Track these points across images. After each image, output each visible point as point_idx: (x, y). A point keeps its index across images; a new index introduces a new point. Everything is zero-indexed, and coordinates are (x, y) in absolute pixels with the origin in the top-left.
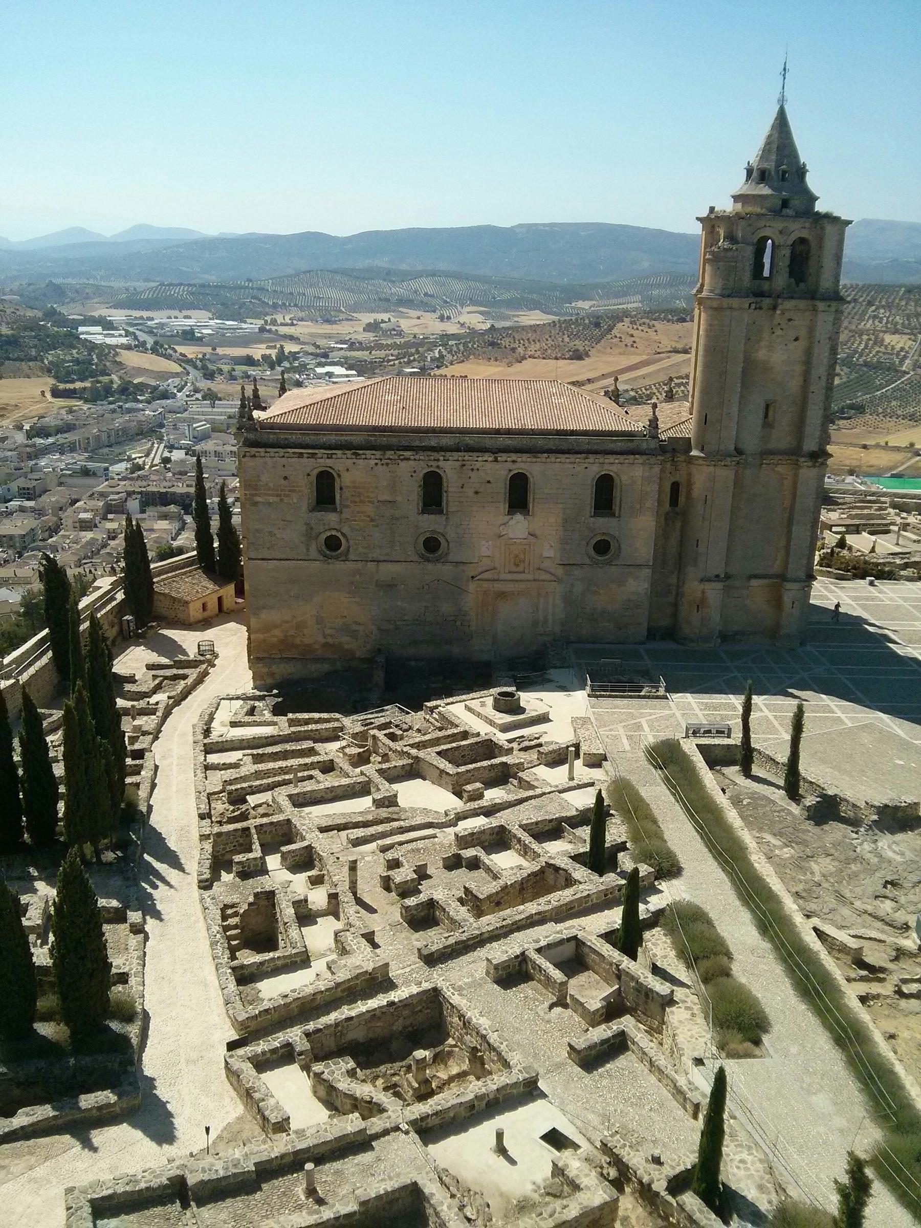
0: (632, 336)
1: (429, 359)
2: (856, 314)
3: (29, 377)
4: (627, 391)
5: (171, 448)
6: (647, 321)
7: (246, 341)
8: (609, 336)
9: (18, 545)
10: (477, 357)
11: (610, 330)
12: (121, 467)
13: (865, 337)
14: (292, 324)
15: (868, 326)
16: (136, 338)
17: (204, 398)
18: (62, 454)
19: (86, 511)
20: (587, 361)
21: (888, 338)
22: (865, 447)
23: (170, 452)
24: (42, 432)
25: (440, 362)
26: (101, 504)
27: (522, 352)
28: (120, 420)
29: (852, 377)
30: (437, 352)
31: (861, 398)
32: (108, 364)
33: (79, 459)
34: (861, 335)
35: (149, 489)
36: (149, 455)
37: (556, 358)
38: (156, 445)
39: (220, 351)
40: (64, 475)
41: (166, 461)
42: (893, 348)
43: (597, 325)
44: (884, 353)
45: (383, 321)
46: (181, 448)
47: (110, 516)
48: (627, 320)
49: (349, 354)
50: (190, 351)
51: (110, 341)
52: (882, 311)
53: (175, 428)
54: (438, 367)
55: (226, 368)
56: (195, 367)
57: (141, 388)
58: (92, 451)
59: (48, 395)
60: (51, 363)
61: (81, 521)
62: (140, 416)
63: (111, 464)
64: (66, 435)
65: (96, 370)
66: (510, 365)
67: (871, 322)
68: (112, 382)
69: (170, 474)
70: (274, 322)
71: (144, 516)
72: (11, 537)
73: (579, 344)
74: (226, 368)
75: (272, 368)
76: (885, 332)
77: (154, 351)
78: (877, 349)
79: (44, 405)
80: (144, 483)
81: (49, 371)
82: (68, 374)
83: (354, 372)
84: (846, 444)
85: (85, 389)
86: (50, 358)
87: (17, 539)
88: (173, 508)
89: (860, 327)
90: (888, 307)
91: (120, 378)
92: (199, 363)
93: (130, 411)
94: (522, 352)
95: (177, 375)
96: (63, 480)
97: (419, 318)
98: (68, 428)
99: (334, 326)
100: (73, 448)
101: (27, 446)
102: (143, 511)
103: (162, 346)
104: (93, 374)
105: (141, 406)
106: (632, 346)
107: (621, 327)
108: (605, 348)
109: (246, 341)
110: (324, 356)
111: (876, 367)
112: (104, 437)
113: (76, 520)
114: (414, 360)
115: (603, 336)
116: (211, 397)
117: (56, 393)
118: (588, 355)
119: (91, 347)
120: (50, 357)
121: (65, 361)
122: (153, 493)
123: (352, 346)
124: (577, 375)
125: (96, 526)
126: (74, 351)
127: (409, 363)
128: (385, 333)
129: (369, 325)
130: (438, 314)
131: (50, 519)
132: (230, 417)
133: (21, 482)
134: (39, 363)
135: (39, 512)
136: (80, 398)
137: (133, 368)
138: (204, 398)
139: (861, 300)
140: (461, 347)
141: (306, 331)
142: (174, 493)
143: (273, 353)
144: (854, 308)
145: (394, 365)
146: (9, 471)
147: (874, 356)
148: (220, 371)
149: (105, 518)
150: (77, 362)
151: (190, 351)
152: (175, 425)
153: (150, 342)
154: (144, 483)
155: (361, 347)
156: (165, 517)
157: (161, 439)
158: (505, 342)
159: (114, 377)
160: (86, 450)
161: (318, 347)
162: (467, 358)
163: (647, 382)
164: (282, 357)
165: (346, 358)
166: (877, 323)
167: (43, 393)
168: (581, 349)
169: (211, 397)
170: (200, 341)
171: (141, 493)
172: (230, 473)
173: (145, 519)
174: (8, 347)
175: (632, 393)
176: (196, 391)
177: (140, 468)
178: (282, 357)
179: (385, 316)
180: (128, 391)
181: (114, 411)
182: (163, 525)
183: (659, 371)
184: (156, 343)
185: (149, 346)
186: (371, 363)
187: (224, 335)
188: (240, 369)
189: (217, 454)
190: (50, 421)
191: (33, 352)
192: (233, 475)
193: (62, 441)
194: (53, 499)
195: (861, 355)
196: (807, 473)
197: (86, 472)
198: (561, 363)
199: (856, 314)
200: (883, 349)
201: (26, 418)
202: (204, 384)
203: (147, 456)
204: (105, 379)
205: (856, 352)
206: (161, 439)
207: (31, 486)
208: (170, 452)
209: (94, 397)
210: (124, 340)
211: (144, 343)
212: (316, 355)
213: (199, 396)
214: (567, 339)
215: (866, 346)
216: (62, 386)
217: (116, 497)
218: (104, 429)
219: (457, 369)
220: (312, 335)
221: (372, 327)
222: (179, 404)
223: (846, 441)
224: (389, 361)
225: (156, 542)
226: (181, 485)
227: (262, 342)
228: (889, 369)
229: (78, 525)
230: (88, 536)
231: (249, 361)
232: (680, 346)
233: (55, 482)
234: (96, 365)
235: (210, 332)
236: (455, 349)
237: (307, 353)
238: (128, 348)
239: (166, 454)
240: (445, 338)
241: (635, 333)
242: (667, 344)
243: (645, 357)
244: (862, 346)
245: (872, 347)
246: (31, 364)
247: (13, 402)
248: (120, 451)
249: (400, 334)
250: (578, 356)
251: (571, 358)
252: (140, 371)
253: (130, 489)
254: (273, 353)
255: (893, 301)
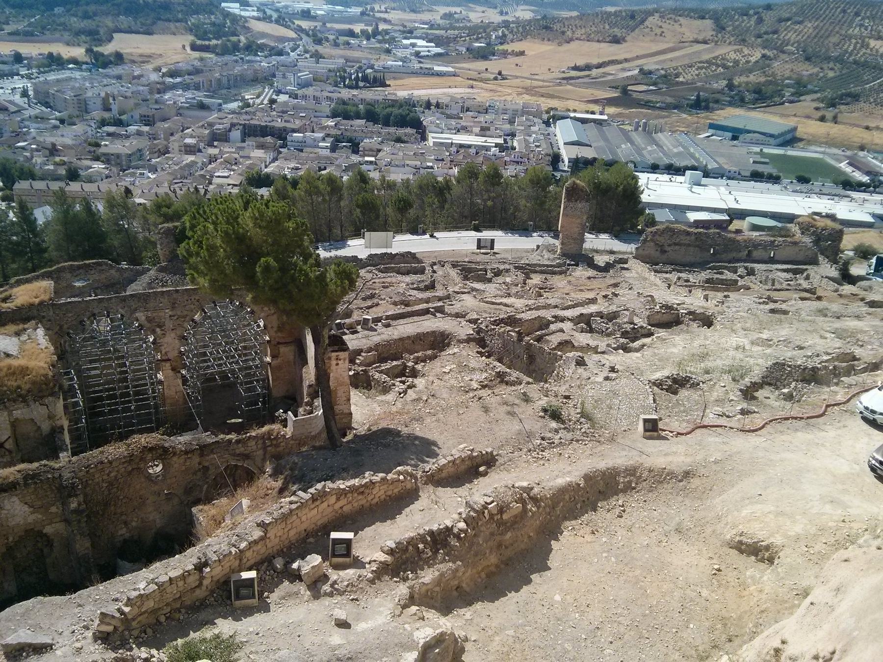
0: (661, 27)
1: (494, 37)
2: (845, 22)
3: (174, 34)
4: (658, 70)
5: (279, 92)
6: (673, 16)
7: (352, 20)
8: (642, 27)
9: (124, 163)
10: (534, 37)
11: (643, 21)
12: (234, 105)
13: (854, 41)
14: (386, 12)
15: (856, 31)
16: (265, 13)
17: (311, 57)
18: (184, 91)
19: (192, 136)
20: (624, 45)
21: (873, 43)
22: (867, 128)
23: (277, 95)
24: (172, 74)
25: (503, 40)
26: (207, 132)
27: (570, 35)
28: (239, 68)
29: (844, 72)
30: (500, 32)
31: (854, 89)
32: (238, 28)
33: (200, 96)
34: (849, 40)
35: (252, 122)
36: (258, 97)
37: (598, 41)
38: (267, 90)
39: (328, 25)
40: (181, 108)
41: (272, 102)
42: (877, 51)
43: (632, 17)
44: (870, 55)
45: (456, 13)
46: (287, 93)
47: (216, 143)
48: (657, 15)
49: (430, 32)
50: (305, 24)
51: (243, 13)
52: (867, 21)
53: (284, 76)
54: (501, 44)
55: (331, 37)
56: (308, 35)
57: (262, 47)
58: (213, 92)
59: (188, 49)
60: (193, 24)
61: (187, 146)
62: (256, 66)
63: (225, 103)
64: (192, 77)
65: (228, 32)
66: (560, 44)
67: (858, 29)
68: (239, 41)
69: (275, 113)
70: (372, 9)
71: (243, 145)
72: (118, 156)
73: (617, 32)
74: (331, 37)
75: (368, 39)
76: (870, 38)
77: (277, 22)
78: (864, 51)
79: (183, 56)
80: (249, 117)
81: (191, 30)
82: (205, 33)
83: (433, 44)
84: (850, 125)
85: (217, 45)
86: (193, 21)
87: (124, 158)
88: (269, 139)
89: (849, 32)
90: (873, 18)
91: (247, 38)
92: (311, 32)
93: (249, 61)
94: (570, 35)
95: (292, 39)
96: (181, 111)
97: (483, 12)
98: (197, 71)
99: (418, 15)
100: (197, 87)
101: (158, 83)
102: (243, 141)
103: (284, 19)
104: (226, 35)
105: (258, 58)
106: (661, 35)
107: (652, 21)
108: (638, 35)
109: (352, 20)
110: (409, 33)
111: (865, 65)
112: (224, 80)
113: (182, 144)
114: (482, 37)
115: (637, 26)
116: (317, 56)
117: (194, 48)
118: (626, 41)
119: (227, 15)
120: (193, 20)
121: (205, 24)
122: (255, 126)
123: (432, 27)
124: (616, 55)
125: (200, 151)
126: (212, 17)
127: (477, 40)
128: (457, 21)
129: (445, 14)
130: (498, 10)
131: (160, 143)
132: (330, 71)
133: (143, 110)
134: (183, 24)
135: (153, 137)
136: (213, 52)
137: (259, 32)
138: (311, 57)
139: (849, 11)
140: (520, 29)
141: (397, 17)
142: (273, 127)
143: (370, 29)
144: (843, 17)
145: (465, 41)
146: (137, 101)
147: (861, 56)
148: (327, 39)
149: (210, 145)
150: (213, 24)
151: (305, 24)
152: (284, 75)
153: (275, 16)
154: (249, 117)
155: (439, 27)
156: (261, 146)
157: (272, 85)
158: (557, 27)
159: (242, 38)
160: (208, 91)
161: (405, 27)
162: (525, 38)
163: (674, 64)
164: (376, 33)
165: (427, 34)
166: (863, 30)
167: (184, 47)
168: (619, 35)
169: (317, 56)
170: (314, 18)
171: (244, 125)
172: (325, 115)
173: (244, 148)
174: (161, 10)
175: (663, 72)
176: (306, 52)
177: (248, 105)
178: (376, 33)
179: (458, 10)
180: (252, 48)
181: (236, 61)
182: (259, 153)
183: (683, 56)
184: (279, 17)
185: (273, 19)
186: (447, 37)
187: (333, 16)
188: (343, 39)
189: (315, 98)
190: (182, 66)
191: (180, 16)
192: (327, 117)
193: (188, 81)
194: (166, 126)
195: (851, 55)
196: (10, 261)
197: (202, 106)
198: (603, 45)
199: (845, 22)
200: (868, 51)
201: (166, 64)
202: (313, 48)
203: (258, 97)
204: (234, 39)
205: (846, 51)
206: (272, 85)
207: (151, 114)
208: (277, 95)
209: (225, 51)
210: (255, 14)
211: (271, 16)
212: (404, 32)
213: (308, 56)
214: (607, 27)
215: (855, 48)
216: (199, 42)
217: (221, 127)
218: (225, 74)
219: (516, 47)
220: (401, 20)
221: (446, 16)
222: (290, 60)
223: (848, 121)
224: (461, 37)
225: (248, 168)
226: (279, 120)
227: (361, 22)
228: (874, 67)
229: (183, 149)
230: (191, 158)
231: (351, 34)
232: (700, 38)
233: (174, 112)
234: (229, 28)
235: (323, 13)
236: (515, 30)
237: (395, 31)
238: (254, 18)
239: (274, 97)
240: (506, 24)
241: (664, 25)
242: (689, 36)
243: (671, 45)
244: (851, 48)
245: (860, 49)
246: (178, 24)
247: (158, 52)
248: (236, 92)
249: (470, 21)
250: (616, 40)
251: (610, 42)
252: (264, 35)
253: (235, 121)
254: (370, 29)
255: (877, 14)
